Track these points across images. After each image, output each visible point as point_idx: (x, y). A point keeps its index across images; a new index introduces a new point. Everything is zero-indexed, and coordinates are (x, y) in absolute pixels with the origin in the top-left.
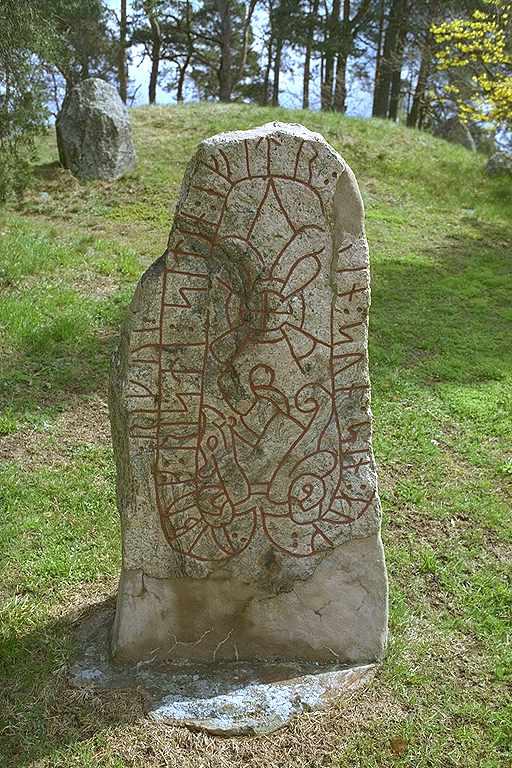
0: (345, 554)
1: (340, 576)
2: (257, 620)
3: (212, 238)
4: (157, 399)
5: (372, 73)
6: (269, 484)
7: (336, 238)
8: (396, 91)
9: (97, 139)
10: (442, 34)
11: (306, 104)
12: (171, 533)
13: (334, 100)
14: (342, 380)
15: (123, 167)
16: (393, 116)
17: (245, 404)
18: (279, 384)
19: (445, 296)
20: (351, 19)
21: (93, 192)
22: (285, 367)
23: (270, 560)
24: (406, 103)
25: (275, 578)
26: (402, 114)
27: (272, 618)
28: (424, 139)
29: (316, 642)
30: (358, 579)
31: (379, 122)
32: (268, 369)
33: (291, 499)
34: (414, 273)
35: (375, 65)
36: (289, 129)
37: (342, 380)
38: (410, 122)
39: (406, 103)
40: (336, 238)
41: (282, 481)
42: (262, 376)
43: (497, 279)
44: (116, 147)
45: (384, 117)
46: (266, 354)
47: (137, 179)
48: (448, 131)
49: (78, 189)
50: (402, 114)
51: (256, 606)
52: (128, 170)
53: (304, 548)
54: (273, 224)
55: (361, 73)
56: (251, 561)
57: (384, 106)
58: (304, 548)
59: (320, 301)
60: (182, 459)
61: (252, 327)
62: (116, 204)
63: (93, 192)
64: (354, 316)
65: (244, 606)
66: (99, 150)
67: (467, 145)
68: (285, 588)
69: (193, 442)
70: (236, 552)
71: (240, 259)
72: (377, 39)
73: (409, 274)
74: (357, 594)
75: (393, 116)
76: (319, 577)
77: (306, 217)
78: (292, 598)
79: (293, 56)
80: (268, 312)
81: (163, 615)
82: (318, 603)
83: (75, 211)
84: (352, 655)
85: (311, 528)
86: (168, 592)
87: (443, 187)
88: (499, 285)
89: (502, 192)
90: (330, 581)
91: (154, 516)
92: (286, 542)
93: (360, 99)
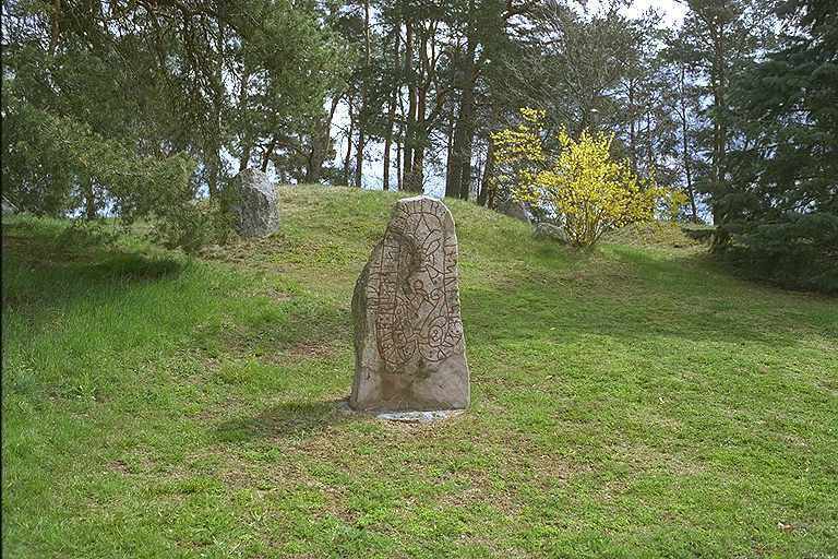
0: (450, 360)
1: (449, 371)
2: (415, 391)
3: (401, 234)
4: (379, 294)
5: (445, 160)
6: (421, 330)
7: (445, 234)
8: (467, 178)
9: (254, 210)
10: (498, 140)
11: (386, 186)
12: (381, 350)
13: (413, 182)
14: (448, 288)
15: (271, 228)
16: (465, 196)
17: (412, 296)
18: (425, 288)
19: (502, 306)
20: (426, 117)
21: (252, 245)
22: (427, 281)
23: (421, 364)
24: (476, 187)
25: (423, 373)
26: (473, 196)
27: (420, 389)
28: (489, 214)
29: (440, 399)
30: (456, 372)
31: (449, 200)
32: (421, 282)
33: (429, 336)
34: (479, 296)
35: (447, 153)
36: (427, 197)
37: (448, 288)
38: (480, 201)
39: (476, 187)
40: (445, 234)
41: (426, 328)
42: (419, 284)
43: (535, 298)
44: (268, 215)
45: (458, 197)
46: (421, 276)
47: (283, 236)
48: (508, 208)
49: (241, 244)
50: (473, 196)
51: (415, 384)
52: (275, 231)
53: (434, 358)
54: (423, 229)
55: (435, 161)
56: (413, 364)
57: (457, 187)
58: (434, 358)
59: (440, 258)
60: (388, 318)
61: (416, 265)
62: (271, 253)
63: (252, 245)
64: (453, 263)
65: (410, 385)
66: (255, 217)
67: (524, 219)
68: (427, 376)
69: (392, 311)
70: (407, 360)
71: (411, 242)
72: (449, 133)
73: (478, 295)
74: (457, 379)
75: (465, 196)
76: (441, 370)
77: (435, 227)
78: (430, 380)
79: (375, 148)
80: (421, 261)
81: (376, 388)
82: (441, 382)
83: (241, 257)
84: (456, 405)
85: (437, 349)
86: (378, 377)
87: (507, 245)
88: (537, 301)
89: (548, 257)
90: (445, 372)
91: (375, 343)
92: (427, 355)
93: (435, 185)
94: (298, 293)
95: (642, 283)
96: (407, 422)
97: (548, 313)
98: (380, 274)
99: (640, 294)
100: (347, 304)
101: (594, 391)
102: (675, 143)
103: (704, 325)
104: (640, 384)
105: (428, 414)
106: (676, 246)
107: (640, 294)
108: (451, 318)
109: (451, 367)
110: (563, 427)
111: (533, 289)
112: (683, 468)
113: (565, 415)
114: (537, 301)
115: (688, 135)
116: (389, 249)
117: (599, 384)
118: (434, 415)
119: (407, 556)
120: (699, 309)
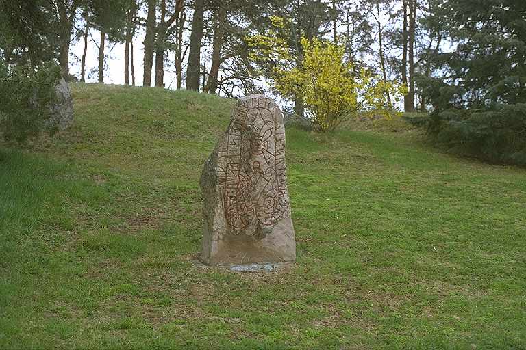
23: (258, 228)
25: (260, 233)
32: (258, 162)
42: (257, 165)
54: (259, 121)
88: (304, 178)
94: (111, 176)
95: (380, 162)
96: (254, 272)
97: (317, 187)
98: (227, 157)
99: (382, 171)
100: (194, 184)
101: (383, 244)
102: (372, 41)
103: (441, 193)
104: (415, 238)
105: (268, 267)
106: (395, 131)
107: (382, 171)
108: (280, 191)
109: (282, 229)
110: (372, 272)
111: (298, 168)
112: (471, 295)
113: (370, 262)
114: (304, 178)
115: (383, 35)
116: (234, 136)
117: (385, 239)
118: (273, 266)
119: (509, 348)
120: (432, 181)
